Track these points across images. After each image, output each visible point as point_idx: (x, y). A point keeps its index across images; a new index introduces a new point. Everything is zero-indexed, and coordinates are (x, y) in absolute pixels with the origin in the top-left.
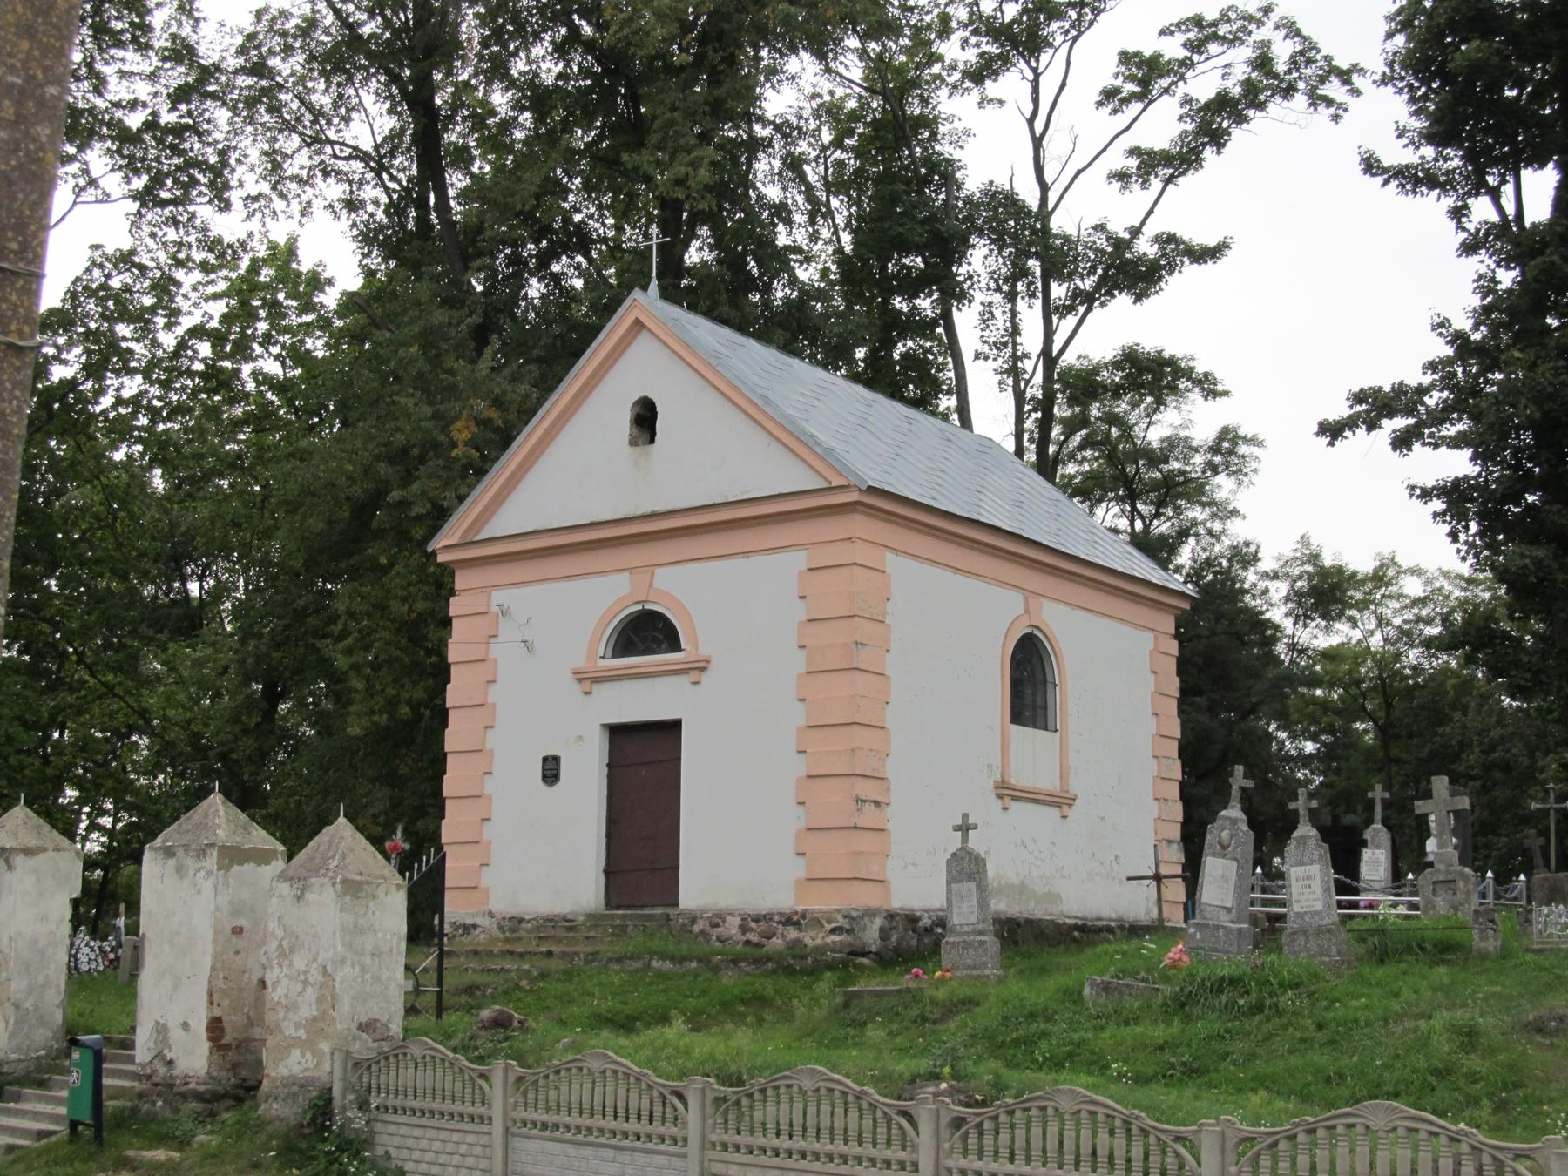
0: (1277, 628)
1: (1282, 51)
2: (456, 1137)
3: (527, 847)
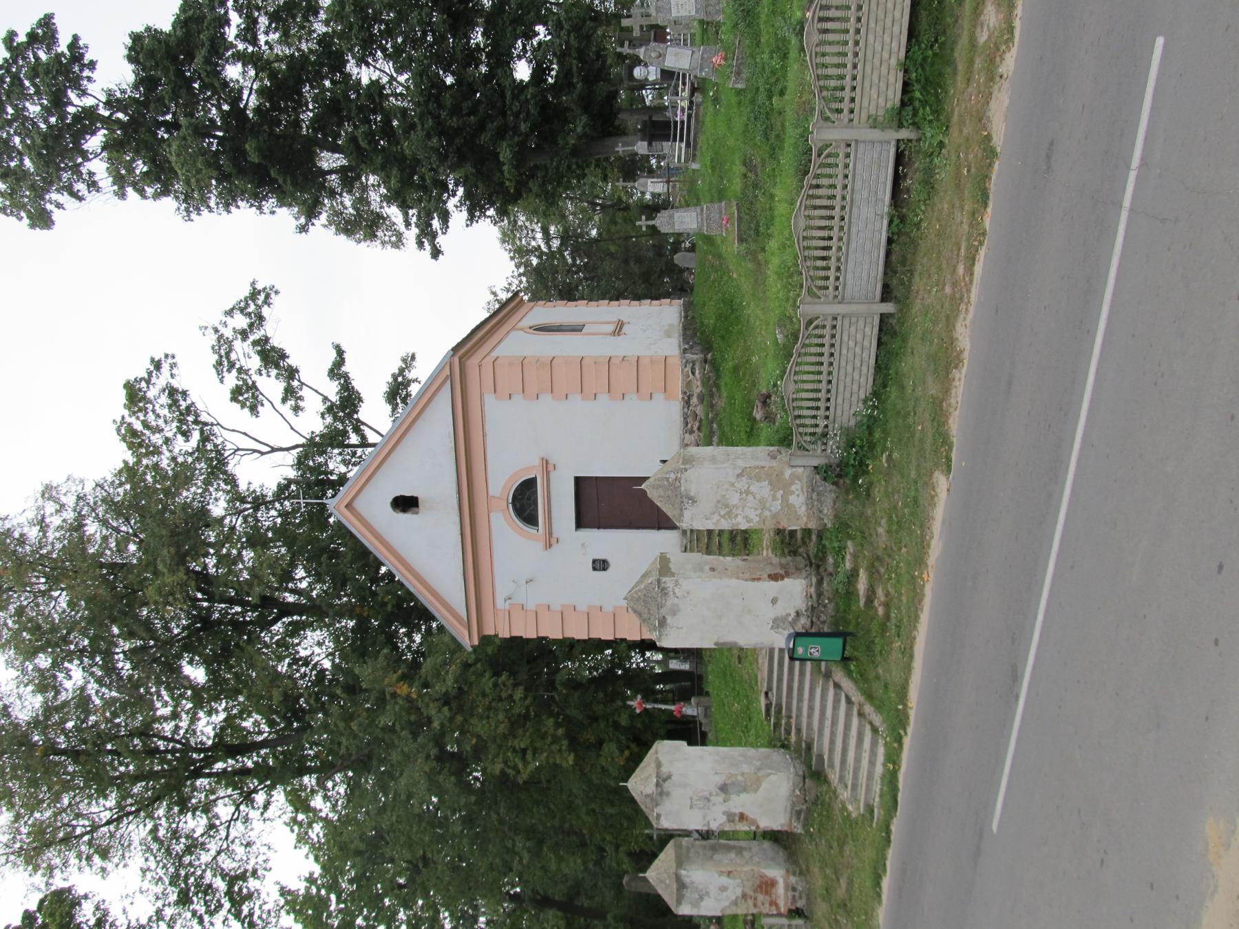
1: (241, 322)
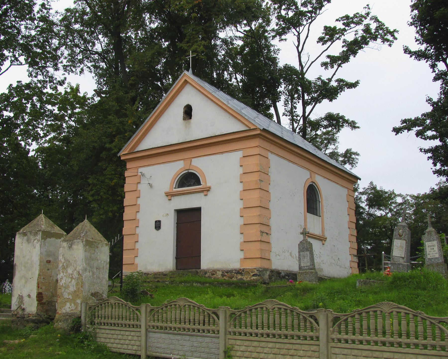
0: (364, 209)
1: (373, 26)
2: (127, 333)
3: (152, 250)
